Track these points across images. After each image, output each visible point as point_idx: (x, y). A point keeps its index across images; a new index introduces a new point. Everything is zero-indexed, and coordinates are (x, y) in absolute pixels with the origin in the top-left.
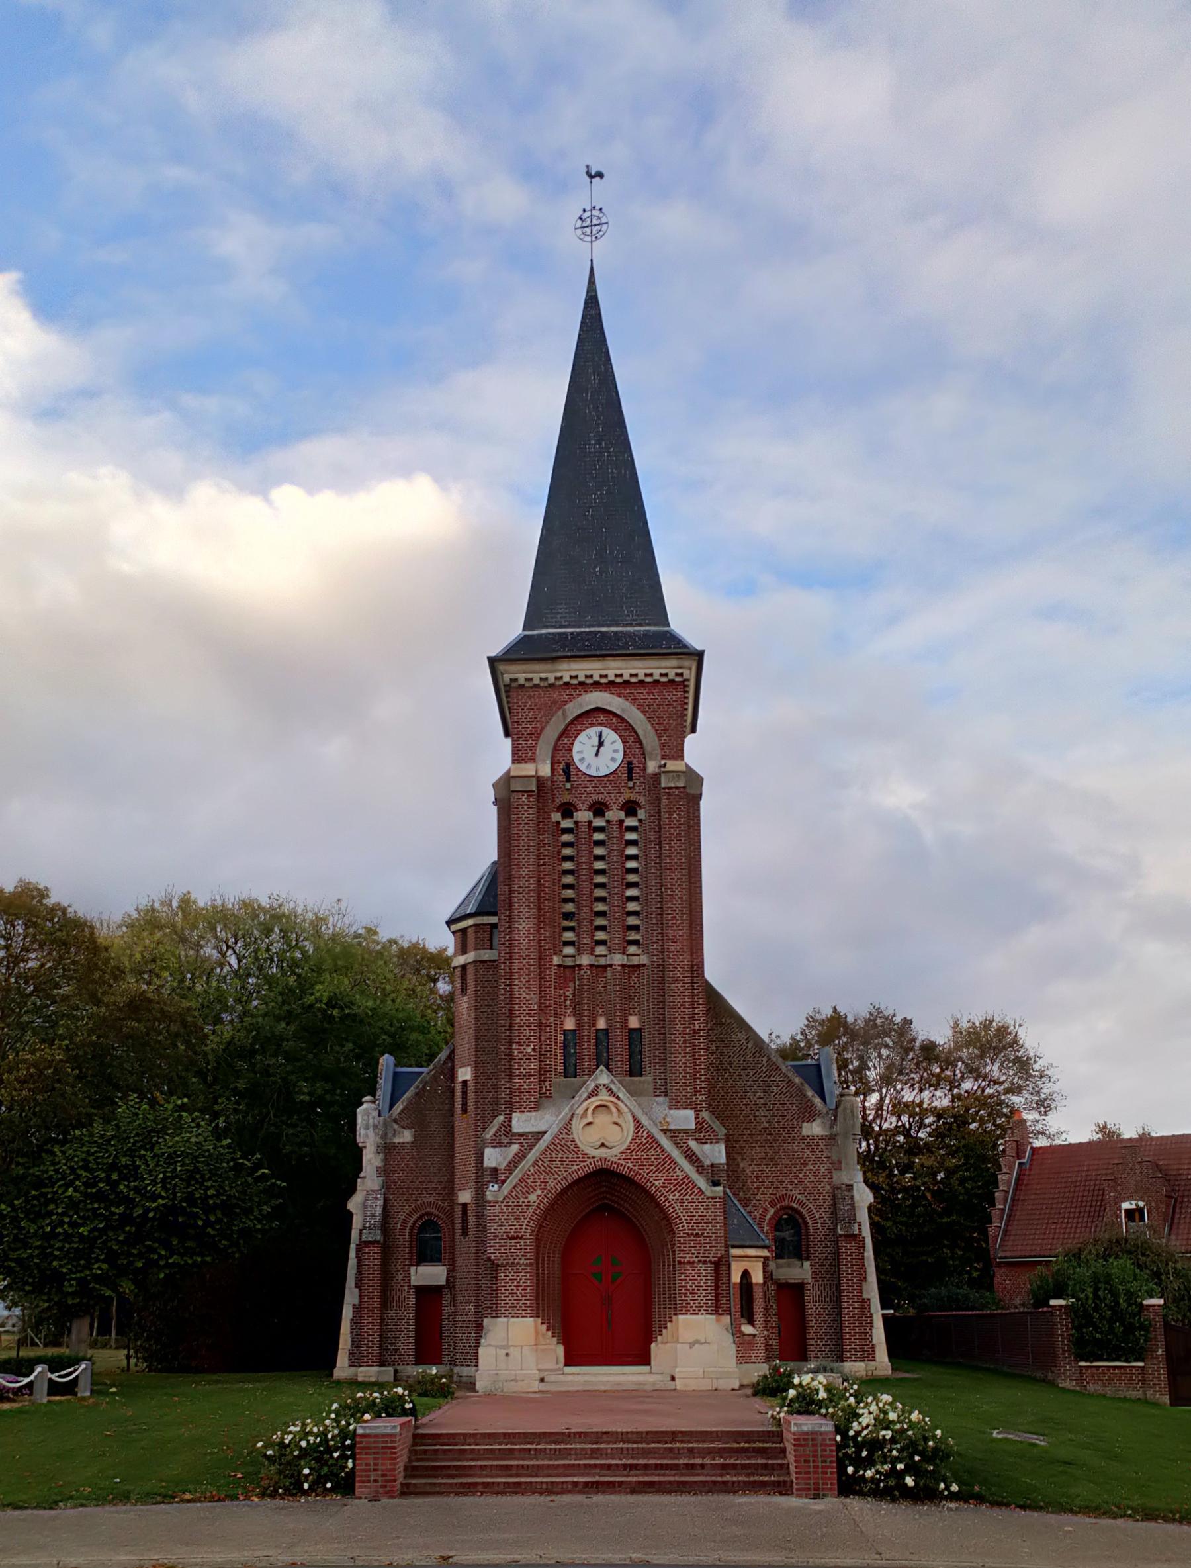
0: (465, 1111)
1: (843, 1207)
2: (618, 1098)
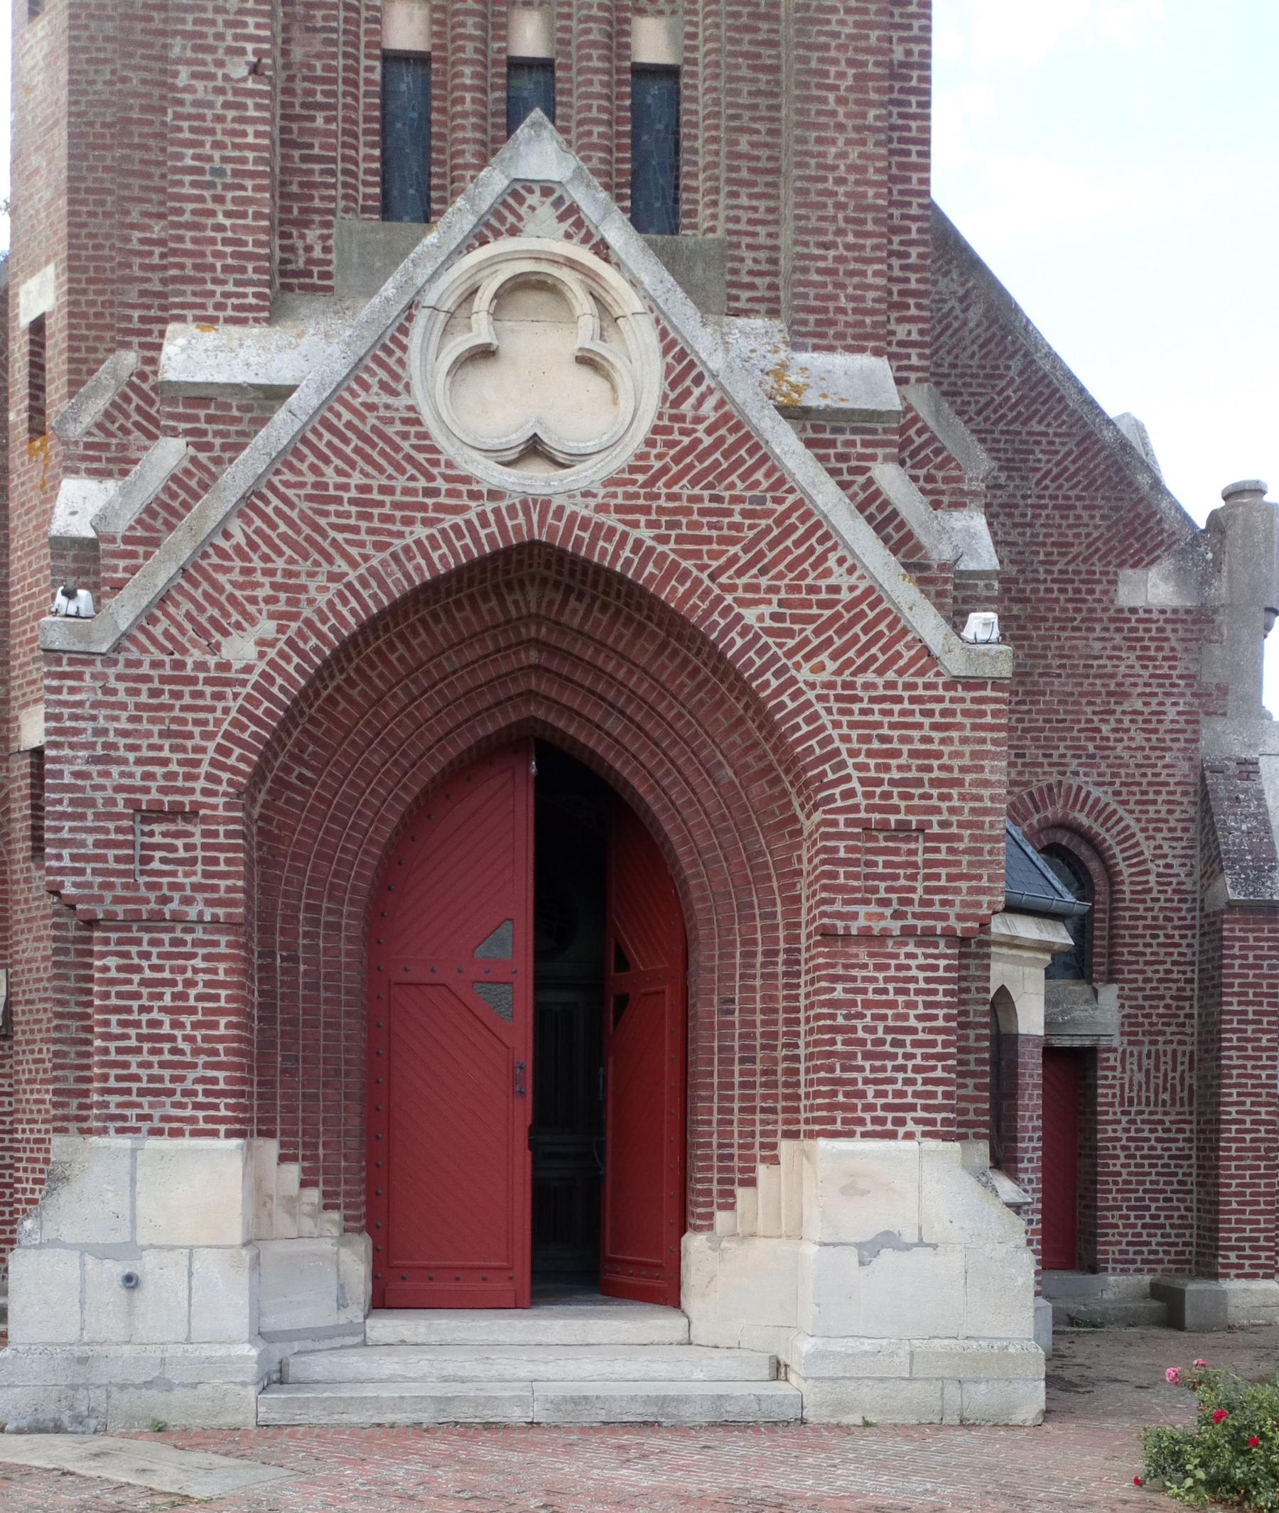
2: (602, 249)
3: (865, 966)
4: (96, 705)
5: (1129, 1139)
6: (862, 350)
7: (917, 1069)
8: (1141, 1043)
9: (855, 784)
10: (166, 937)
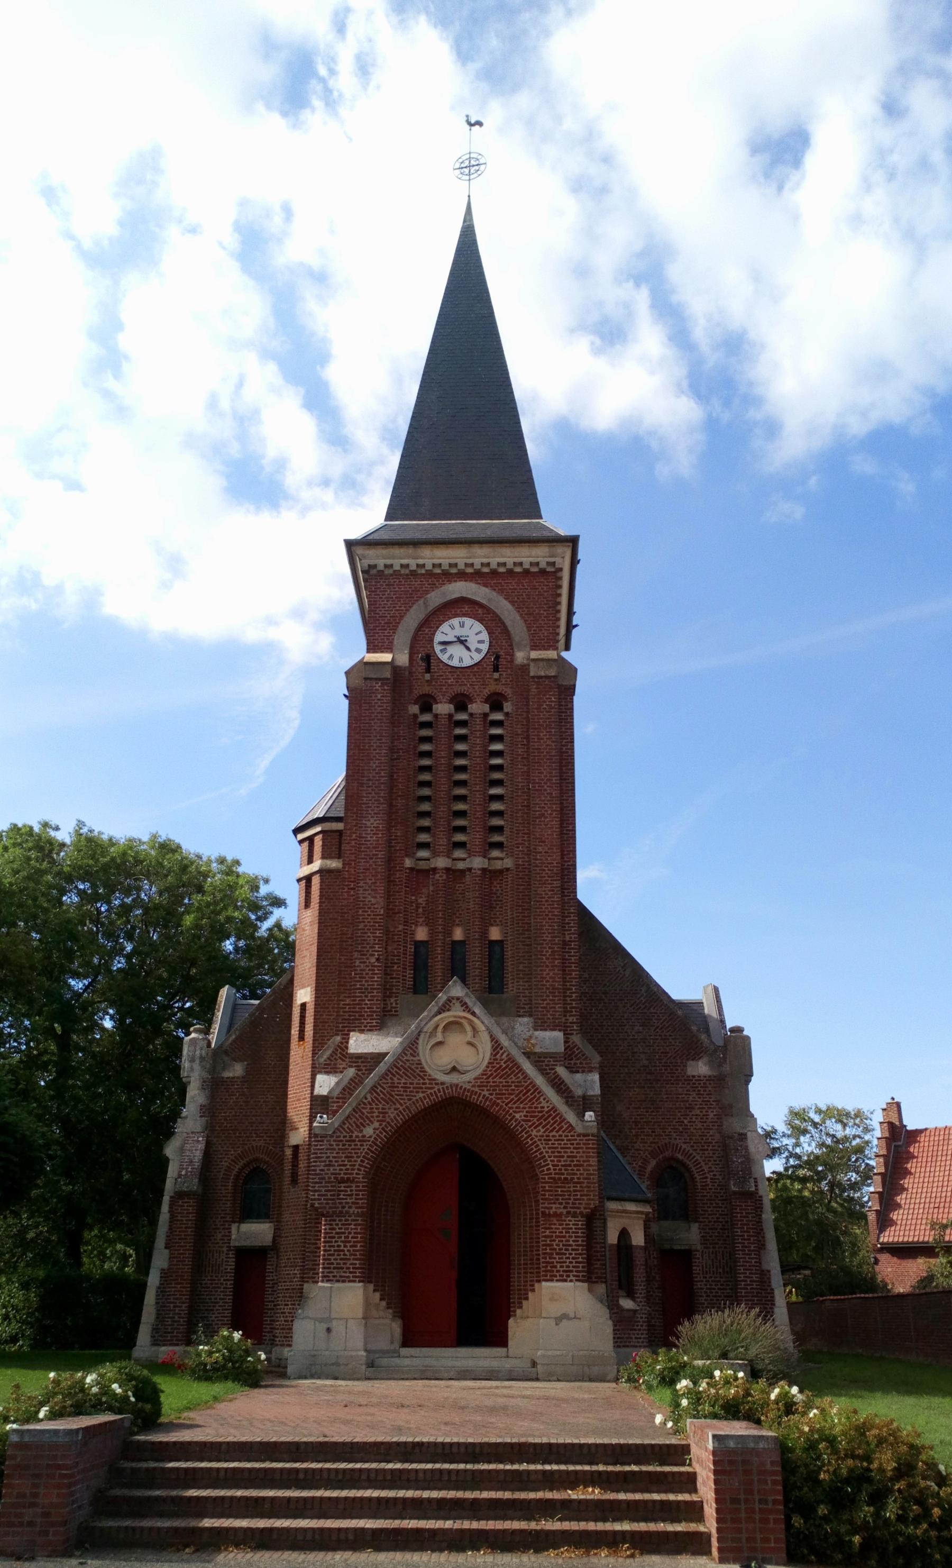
0: (301, 1038)
1: (737, 1160)
2: (474, 1014)
3: (555, 1224)
4: (327, 1149)
5: (707, 1289)
6: (555, 1030)
7: (573, 1258)
8: (709, 1248)
9: (550, 1166)
10: (343, 1219)
